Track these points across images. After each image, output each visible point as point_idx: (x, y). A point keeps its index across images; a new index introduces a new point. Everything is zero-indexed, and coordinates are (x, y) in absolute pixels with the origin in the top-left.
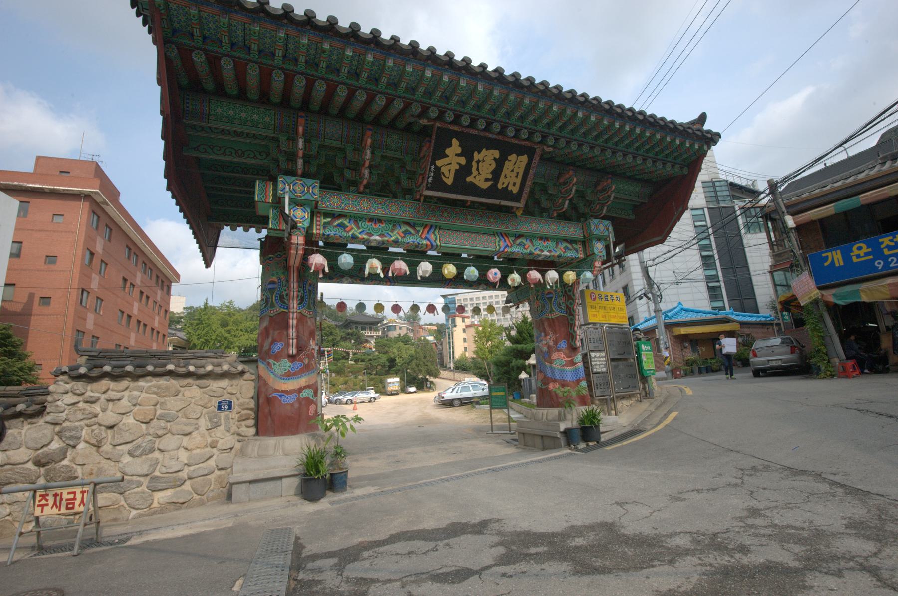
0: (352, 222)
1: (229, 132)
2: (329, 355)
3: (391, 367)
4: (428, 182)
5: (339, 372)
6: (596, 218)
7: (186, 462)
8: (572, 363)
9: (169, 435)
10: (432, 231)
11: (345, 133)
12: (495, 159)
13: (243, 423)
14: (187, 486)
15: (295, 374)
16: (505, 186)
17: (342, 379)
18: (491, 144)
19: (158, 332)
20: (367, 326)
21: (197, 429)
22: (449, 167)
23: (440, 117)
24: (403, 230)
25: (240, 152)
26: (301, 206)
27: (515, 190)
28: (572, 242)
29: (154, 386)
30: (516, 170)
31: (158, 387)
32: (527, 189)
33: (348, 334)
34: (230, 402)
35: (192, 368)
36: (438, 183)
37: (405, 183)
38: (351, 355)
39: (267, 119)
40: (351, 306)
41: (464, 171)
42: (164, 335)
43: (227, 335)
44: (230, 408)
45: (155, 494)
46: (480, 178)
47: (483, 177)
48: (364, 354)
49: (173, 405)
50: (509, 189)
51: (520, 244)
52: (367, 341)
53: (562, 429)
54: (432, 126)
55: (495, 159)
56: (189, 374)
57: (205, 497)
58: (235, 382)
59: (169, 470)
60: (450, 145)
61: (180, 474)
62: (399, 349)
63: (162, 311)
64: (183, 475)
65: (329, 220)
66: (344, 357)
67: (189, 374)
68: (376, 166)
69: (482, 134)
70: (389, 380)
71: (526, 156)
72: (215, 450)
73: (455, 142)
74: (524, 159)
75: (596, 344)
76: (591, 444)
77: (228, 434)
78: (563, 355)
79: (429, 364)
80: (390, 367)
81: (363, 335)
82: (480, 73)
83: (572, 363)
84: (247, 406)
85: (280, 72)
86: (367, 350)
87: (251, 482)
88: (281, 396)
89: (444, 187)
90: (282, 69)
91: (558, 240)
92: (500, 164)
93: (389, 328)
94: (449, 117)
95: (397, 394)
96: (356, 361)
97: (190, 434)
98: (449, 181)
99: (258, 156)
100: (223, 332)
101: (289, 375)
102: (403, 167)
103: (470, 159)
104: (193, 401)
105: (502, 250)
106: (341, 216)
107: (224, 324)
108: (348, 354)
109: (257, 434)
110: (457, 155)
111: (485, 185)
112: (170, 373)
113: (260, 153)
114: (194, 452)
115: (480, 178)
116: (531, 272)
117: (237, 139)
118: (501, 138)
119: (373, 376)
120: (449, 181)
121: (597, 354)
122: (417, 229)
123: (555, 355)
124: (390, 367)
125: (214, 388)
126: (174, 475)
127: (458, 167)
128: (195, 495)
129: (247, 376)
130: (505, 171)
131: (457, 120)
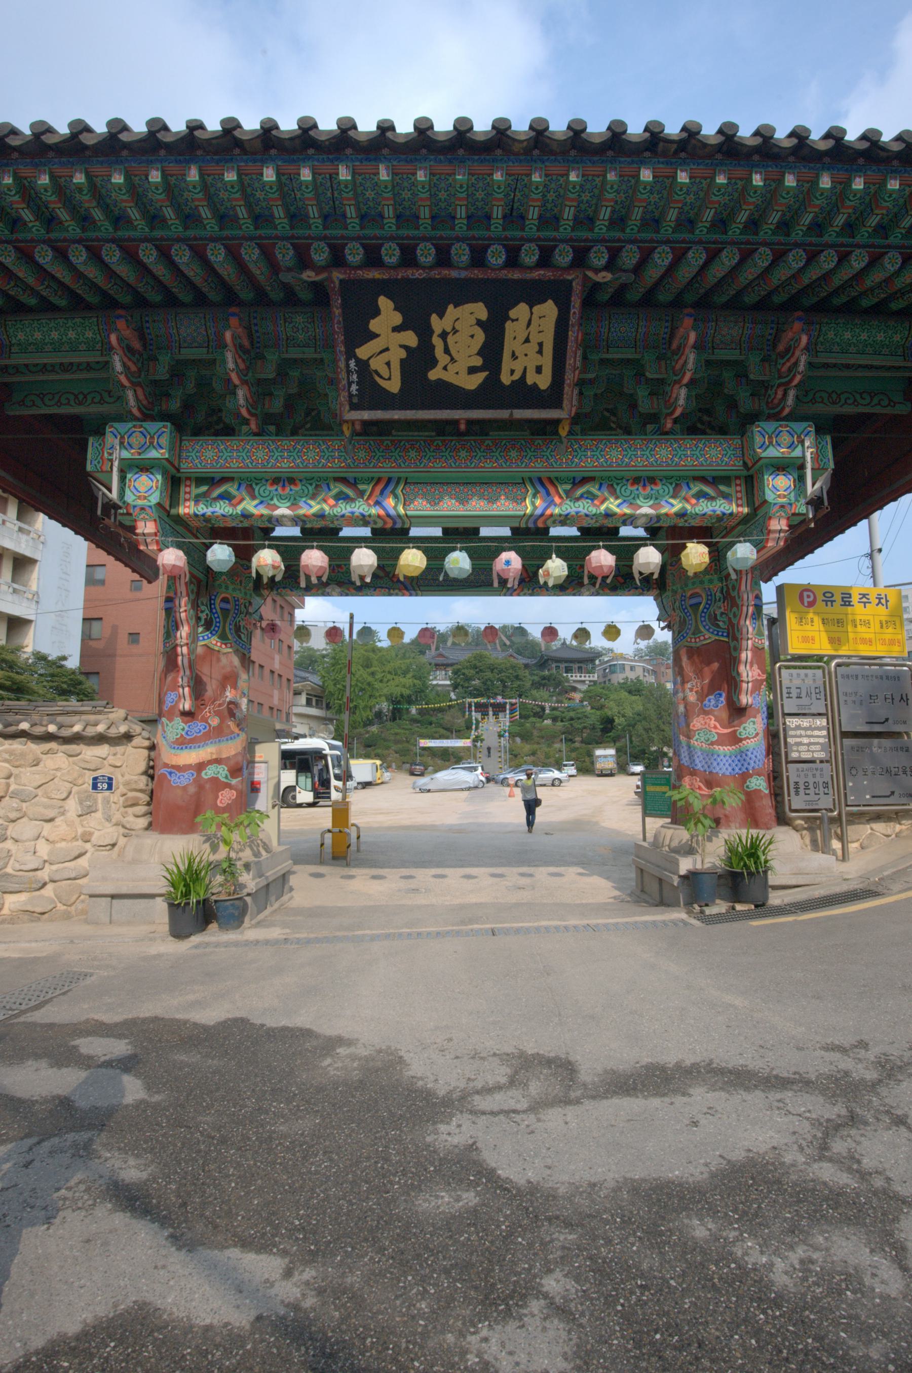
0: (604, 487)
1: (835, 365)
2: (512, 711)
3: (606, 730)
4: (351, 396)
5: (526, 737)
6: (771, 417)
7: (46, 858)
8: (734, 739)
9: (25, 820)
10: (390, 488)
11: (211, 331)
12: (479, 323)
13: (130, 810)
14: (48, 891)
15: (192, 741)
16: (516, 377)
17: (527, 748)
18: (462, 293)
19: (280, 676)
20: (576, 666)
21: (63, 814)
22: (385, 357)
23: (338, 259)
24: (335, 491)
25: (81, 397)
26: (783, 470)
27: (544, 381)
28: (715, 480)
29: (6, 751)
30: (535, 339)
31: (11, 753)
32: (570, 377)
33: (544, 678)
34: (110, 779)
35: (52, 728)
36: (371, 393)
37: (645, 405)
38: (547, 711)
39: (89, 334)
40: (566, 633)
41: (419, 360)
42: (289, 680)
43: (370, 679)
44: (110, 787)
45: (6, 896)
46: (458, 367)
47: (463, 363)
48: (569, 709)
49: (29, 778)
50: (529, 382)
51: (221, 497)
52: (574, 689)
53: (683, 872)
54: (330, 279)
55: (479, 323)
56: (49, 737)
57: (73, 908)
58: (120, 749)
59: (23, 867)
60: (377, 312)
61: (39, 873)
62: (619, 703)
63: (285, 648)
64: (44, 875)
65: (204, 488)
66: (536, 715)
67: (49, 737)
68: (591, 382)
69: (435, 274)
70: (599, 752)
71: (550, 303)
72: (88, 846)
73: (384, 303)
74: (549, 310)
75: (805, 701)
76: (739, 907)
77: (107, 824)
78: (713, 722)
79: (666, 728)
80: (605, 731)
81: (567, 680)
82: (756, 150)
83: (734, 739)
84: (134, 786)
85: (46, 247)
86: (571, 704)
87: (113, 897)
88: (170, 773)
89: (382, 399)
90: (113, 241)
91: (677, 482)
92: (494, 330)
93: (613, 669)
94: (354, 254)
95: (611, 775)
96: (555, 719)
97: (51, 820)
98: (394, 385)
99: (107, 399)
100: (365, 676)
101: (182, 743)
102: (640, 375)
103: (424, 333)
104: (59, 774)
105: (538, 512)
106: (585, 480)
107: (367, 664)
108: (543, 709)
109: (150, 826)
110: (396, 329)
111: (472, 382)
112: (23, 734)
113: (861, 394)
114: (58, 845)
115: (458, 367)
116: (594, 554)
117: (67, 376)
118: (477, 274)
119: (577, 745)
120: (394, 385)
121: (805, 722)
122: (361, 487)
123: (697, 723)
124: (605, 731)
125: (88, 758)
126: (31, 874)
127: (403, 354)
128: (59, 905)
129: (137, 741)
130: (509, 345)
131: (373, 259)
